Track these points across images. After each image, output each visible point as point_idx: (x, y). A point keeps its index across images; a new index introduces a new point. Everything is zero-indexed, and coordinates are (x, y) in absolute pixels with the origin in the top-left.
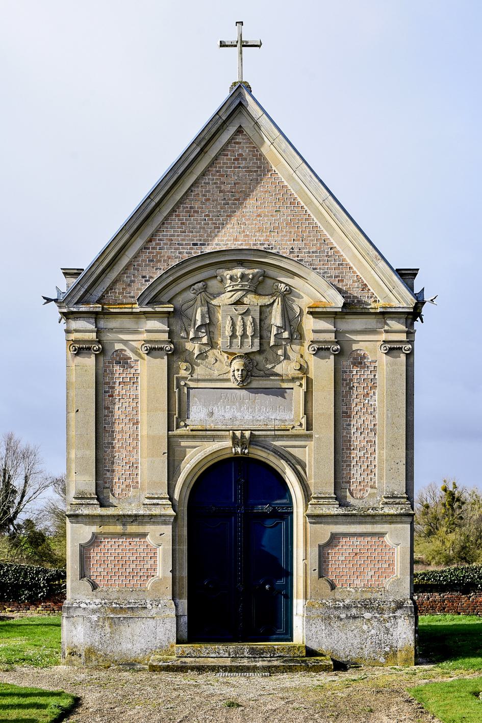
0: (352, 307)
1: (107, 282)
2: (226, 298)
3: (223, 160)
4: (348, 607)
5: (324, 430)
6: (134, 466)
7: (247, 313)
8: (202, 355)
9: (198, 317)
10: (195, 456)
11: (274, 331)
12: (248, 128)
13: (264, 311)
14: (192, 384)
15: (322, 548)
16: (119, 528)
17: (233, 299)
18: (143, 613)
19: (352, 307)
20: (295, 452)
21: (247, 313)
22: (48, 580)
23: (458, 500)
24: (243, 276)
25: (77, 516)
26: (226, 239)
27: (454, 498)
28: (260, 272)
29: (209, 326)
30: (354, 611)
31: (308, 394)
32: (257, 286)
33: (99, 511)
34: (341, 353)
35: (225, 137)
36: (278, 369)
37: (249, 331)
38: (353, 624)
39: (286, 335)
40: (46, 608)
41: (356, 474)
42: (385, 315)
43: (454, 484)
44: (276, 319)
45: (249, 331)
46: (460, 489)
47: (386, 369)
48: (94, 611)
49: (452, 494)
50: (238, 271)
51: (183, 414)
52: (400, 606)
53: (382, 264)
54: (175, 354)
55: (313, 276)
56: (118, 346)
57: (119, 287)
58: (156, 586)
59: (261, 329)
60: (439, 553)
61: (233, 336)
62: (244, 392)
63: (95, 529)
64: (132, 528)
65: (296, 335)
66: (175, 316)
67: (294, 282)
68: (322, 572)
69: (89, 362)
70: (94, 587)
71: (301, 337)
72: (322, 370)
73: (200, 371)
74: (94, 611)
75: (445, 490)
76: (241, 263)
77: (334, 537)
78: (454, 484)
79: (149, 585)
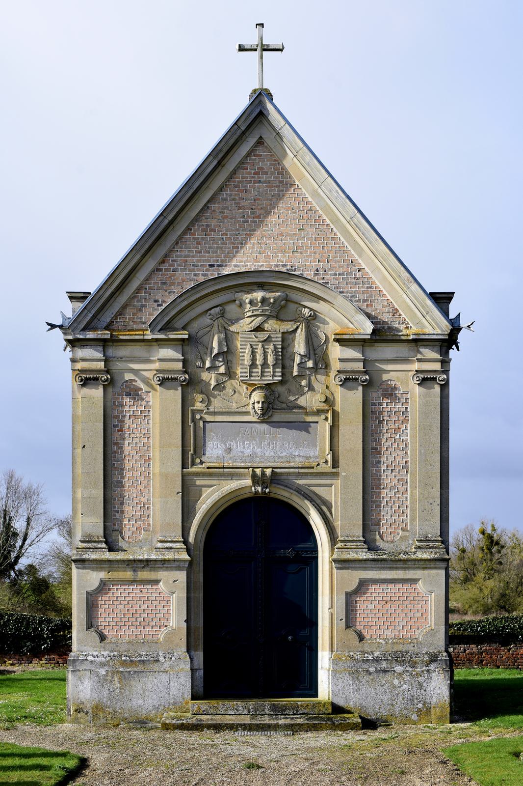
0: (382, 334)
2: (246, 324)
3: (242, 174)
4: (377, 660)
6: (145, 507)
7: (268, 340)
8: (219, 386)
9: (215, 344)
10: (210, 497)
11: (297, 360)
12: (269, 139)
13: (287, 338)
14: (208, 418)
16: (129, 574)
18: (155, 667)
19: (382, 334)
21: (268, 340)
22: (52, 631)
23: (497, 543)
24: (264, 300)
27: (492, 541)
28: (282, 295)
29: (227, 354)
30: (384, 665)
31: (334, 428)
32: (279, 310)
33: (108, 556)
34: (370, 384)
37: (270, 360)
38: (383, 679)
39: (310, 364)
42: (418, 342)
43: (493, 526)
44: (299, 346)
46: (499, 532)
47: (418, 399)
48: (102, 665)
49: (490, 538)
50: (258, 295)
52: (434, 658)
53: (414, 287)
55: (340, 300)
56: (128, 377)
57: (130, 311)
59: (284, 358)
61: (253, 365)
62: (265, 427)
63: (102, 575)
64: (143, 575)
65: (322, 363)
66: (190, 345)
68: (349, 622)
69: (97, 393)
70: (102, 638)
71: (327, 366)
72: (350, 402)
74: (102, 665)
75: (483, 533)
76: (261, 286)
78: (493, 526)
79: (161, 636)
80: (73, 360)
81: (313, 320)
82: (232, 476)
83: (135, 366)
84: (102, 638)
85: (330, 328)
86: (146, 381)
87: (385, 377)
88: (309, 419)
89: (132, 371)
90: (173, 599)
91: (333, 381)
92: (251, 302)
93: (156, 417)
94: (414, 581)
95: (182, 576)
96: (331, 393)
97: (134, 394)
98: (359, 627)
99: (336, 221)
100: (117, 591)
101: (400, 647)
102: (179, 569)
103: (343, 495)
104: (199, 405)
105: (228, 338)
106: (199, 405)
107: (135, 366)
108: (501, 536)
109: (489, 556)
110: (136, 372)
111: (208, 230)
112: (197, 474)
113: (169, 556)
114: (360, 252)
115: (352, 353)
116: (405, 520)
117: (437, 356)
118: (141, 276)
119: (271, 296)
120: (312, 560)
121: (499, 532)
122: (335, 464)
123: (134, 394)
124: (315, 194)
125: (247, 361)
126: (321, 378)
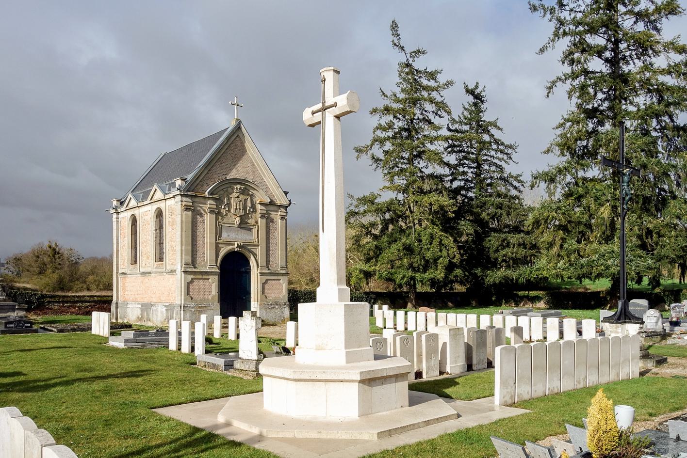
0: (272, 203)
1: (196, 184)
2: (235, 195)
3: (232, 145)
4: (271, 304)
5: (263, 243)
6: (203, 254)
7: (241, 201)
8: (226, 215)
9: (225, 200)
10: (223, 251)
11: (248, 208)
12: (240, 135)
13: (246, 200)
14: (223, 225)
15: (263, 284)
16: (200, 277)
17: (236, 196)
18: (209, 308)
19: (272, 203)
20: (254, 250)
21: (241, 201)
22: (37, 299)
23: (58, 253)
24: (240, 188)
25: (187, 271)
26: (232, 175)
27: (56, 252)
28: (246, 187)
29: (229, 204)
30: (273, 306)
31: (258, 231)
32: (244, 192)
33: (194, 270)
34: (269, 220)
35: (234, 138)
36: (249, 221)
37: (241, 208)
38: (273, 310)
39: (252, 210)
40: (35, 313)
41: (271, 260)
42: (280, 206)
43: (56, 244)
44: (249, 204)
45: (241, 208)
46: (59, 247)
47: (279, 223)
48: (193, 308)
49: (54, 250)
50: (239, 186)
51: (220, 236)
52: (285, 304)
53: (280, 189)
54: (218, 214)
55: (261, 191)
56: (199, 208)
57: (199, 186)
58: (213, 297)
59: (245, 208)
60: (48, 285)
61: (236, 209)
62: (239, 229)
63: (192, 276)
64: (205, 277)
65: (255, 210)
66: (219, 201)
67: (254, 192)
68: (263, 293)
69: (190, 213)
70: (192, 298)
71: (256, 211)
72: (262, 222)
73: (225, 220)
74: (193, 308)
75: (50, 247)
76: (239, 183)
77: (267, 280)
78: (56, 244)
79: (210, 298)
80: (182, 201)
81: (252, 196)
82: (230, 244)
83: (201, 205)
84: (192, 298)
85: (257, 200)
86: (205, 211)
87: (271, 216)
88: (251, 227)
89: (200, 207)
90: (214, 285)
91: (258, 215)
92: (237, 188)
93: (207, 222)
94: (279, 280)
95: (216, 277)
96: (257, 219)
97: (201, 215)
98: (266, 294)
99: (258, 165)
100: (196, 282)
101: (276, 300)
102: (216, 275)
103: (260, 251)
104: (220, 220)
105: (229, 199)
106: (220, 220)
107: (201, 205)
108: (60, 249)
109: (54, 260)
110: (201, 207)
111: (222, 162)
112: (220, 243)
113: (213, 270)
114: (265, 176)
115: (263, 208)
116: (278, 260)
117: (284, 211)
118: (203, 175)
119: (243, 187)
120: (248, 272)
121: (59, 247)
122: (258, 243)
123: (201, 215)
124: (253, 156)
125: (235, 208)
126: (254, 214)
